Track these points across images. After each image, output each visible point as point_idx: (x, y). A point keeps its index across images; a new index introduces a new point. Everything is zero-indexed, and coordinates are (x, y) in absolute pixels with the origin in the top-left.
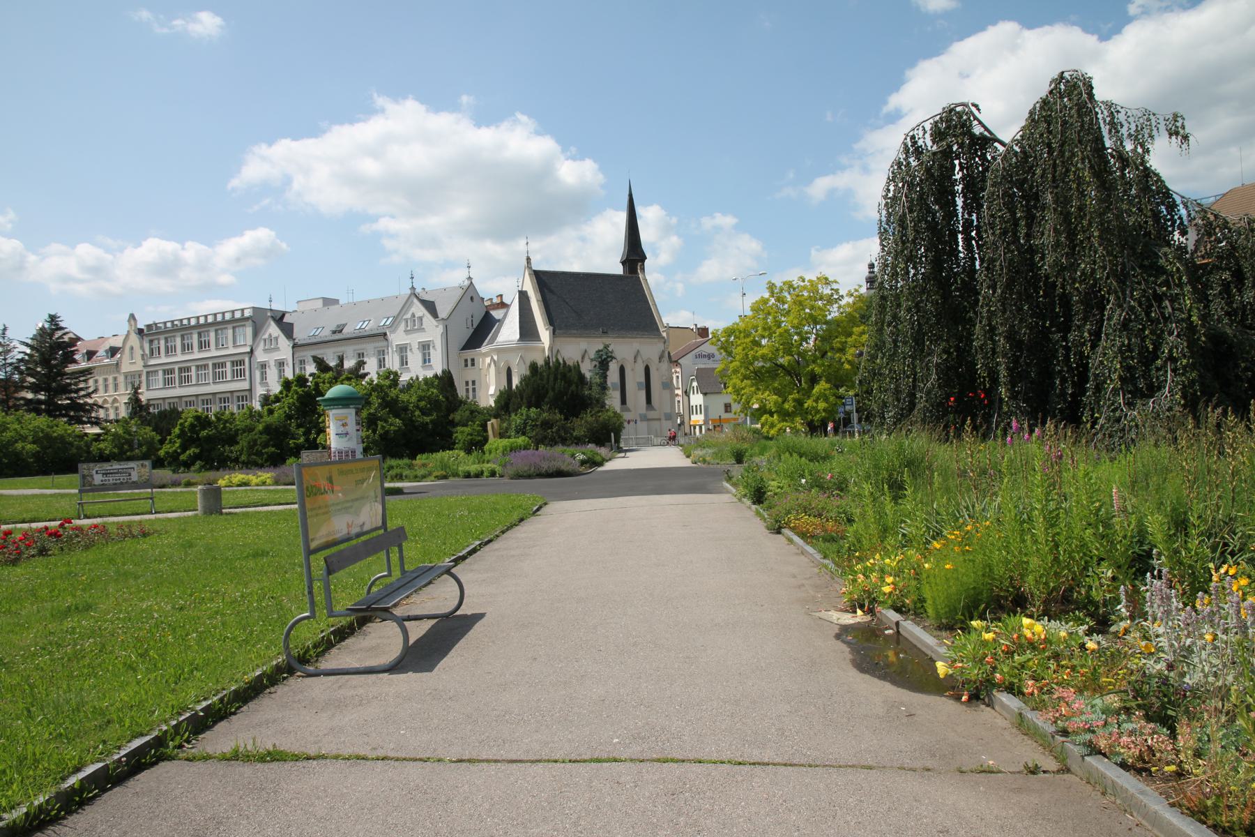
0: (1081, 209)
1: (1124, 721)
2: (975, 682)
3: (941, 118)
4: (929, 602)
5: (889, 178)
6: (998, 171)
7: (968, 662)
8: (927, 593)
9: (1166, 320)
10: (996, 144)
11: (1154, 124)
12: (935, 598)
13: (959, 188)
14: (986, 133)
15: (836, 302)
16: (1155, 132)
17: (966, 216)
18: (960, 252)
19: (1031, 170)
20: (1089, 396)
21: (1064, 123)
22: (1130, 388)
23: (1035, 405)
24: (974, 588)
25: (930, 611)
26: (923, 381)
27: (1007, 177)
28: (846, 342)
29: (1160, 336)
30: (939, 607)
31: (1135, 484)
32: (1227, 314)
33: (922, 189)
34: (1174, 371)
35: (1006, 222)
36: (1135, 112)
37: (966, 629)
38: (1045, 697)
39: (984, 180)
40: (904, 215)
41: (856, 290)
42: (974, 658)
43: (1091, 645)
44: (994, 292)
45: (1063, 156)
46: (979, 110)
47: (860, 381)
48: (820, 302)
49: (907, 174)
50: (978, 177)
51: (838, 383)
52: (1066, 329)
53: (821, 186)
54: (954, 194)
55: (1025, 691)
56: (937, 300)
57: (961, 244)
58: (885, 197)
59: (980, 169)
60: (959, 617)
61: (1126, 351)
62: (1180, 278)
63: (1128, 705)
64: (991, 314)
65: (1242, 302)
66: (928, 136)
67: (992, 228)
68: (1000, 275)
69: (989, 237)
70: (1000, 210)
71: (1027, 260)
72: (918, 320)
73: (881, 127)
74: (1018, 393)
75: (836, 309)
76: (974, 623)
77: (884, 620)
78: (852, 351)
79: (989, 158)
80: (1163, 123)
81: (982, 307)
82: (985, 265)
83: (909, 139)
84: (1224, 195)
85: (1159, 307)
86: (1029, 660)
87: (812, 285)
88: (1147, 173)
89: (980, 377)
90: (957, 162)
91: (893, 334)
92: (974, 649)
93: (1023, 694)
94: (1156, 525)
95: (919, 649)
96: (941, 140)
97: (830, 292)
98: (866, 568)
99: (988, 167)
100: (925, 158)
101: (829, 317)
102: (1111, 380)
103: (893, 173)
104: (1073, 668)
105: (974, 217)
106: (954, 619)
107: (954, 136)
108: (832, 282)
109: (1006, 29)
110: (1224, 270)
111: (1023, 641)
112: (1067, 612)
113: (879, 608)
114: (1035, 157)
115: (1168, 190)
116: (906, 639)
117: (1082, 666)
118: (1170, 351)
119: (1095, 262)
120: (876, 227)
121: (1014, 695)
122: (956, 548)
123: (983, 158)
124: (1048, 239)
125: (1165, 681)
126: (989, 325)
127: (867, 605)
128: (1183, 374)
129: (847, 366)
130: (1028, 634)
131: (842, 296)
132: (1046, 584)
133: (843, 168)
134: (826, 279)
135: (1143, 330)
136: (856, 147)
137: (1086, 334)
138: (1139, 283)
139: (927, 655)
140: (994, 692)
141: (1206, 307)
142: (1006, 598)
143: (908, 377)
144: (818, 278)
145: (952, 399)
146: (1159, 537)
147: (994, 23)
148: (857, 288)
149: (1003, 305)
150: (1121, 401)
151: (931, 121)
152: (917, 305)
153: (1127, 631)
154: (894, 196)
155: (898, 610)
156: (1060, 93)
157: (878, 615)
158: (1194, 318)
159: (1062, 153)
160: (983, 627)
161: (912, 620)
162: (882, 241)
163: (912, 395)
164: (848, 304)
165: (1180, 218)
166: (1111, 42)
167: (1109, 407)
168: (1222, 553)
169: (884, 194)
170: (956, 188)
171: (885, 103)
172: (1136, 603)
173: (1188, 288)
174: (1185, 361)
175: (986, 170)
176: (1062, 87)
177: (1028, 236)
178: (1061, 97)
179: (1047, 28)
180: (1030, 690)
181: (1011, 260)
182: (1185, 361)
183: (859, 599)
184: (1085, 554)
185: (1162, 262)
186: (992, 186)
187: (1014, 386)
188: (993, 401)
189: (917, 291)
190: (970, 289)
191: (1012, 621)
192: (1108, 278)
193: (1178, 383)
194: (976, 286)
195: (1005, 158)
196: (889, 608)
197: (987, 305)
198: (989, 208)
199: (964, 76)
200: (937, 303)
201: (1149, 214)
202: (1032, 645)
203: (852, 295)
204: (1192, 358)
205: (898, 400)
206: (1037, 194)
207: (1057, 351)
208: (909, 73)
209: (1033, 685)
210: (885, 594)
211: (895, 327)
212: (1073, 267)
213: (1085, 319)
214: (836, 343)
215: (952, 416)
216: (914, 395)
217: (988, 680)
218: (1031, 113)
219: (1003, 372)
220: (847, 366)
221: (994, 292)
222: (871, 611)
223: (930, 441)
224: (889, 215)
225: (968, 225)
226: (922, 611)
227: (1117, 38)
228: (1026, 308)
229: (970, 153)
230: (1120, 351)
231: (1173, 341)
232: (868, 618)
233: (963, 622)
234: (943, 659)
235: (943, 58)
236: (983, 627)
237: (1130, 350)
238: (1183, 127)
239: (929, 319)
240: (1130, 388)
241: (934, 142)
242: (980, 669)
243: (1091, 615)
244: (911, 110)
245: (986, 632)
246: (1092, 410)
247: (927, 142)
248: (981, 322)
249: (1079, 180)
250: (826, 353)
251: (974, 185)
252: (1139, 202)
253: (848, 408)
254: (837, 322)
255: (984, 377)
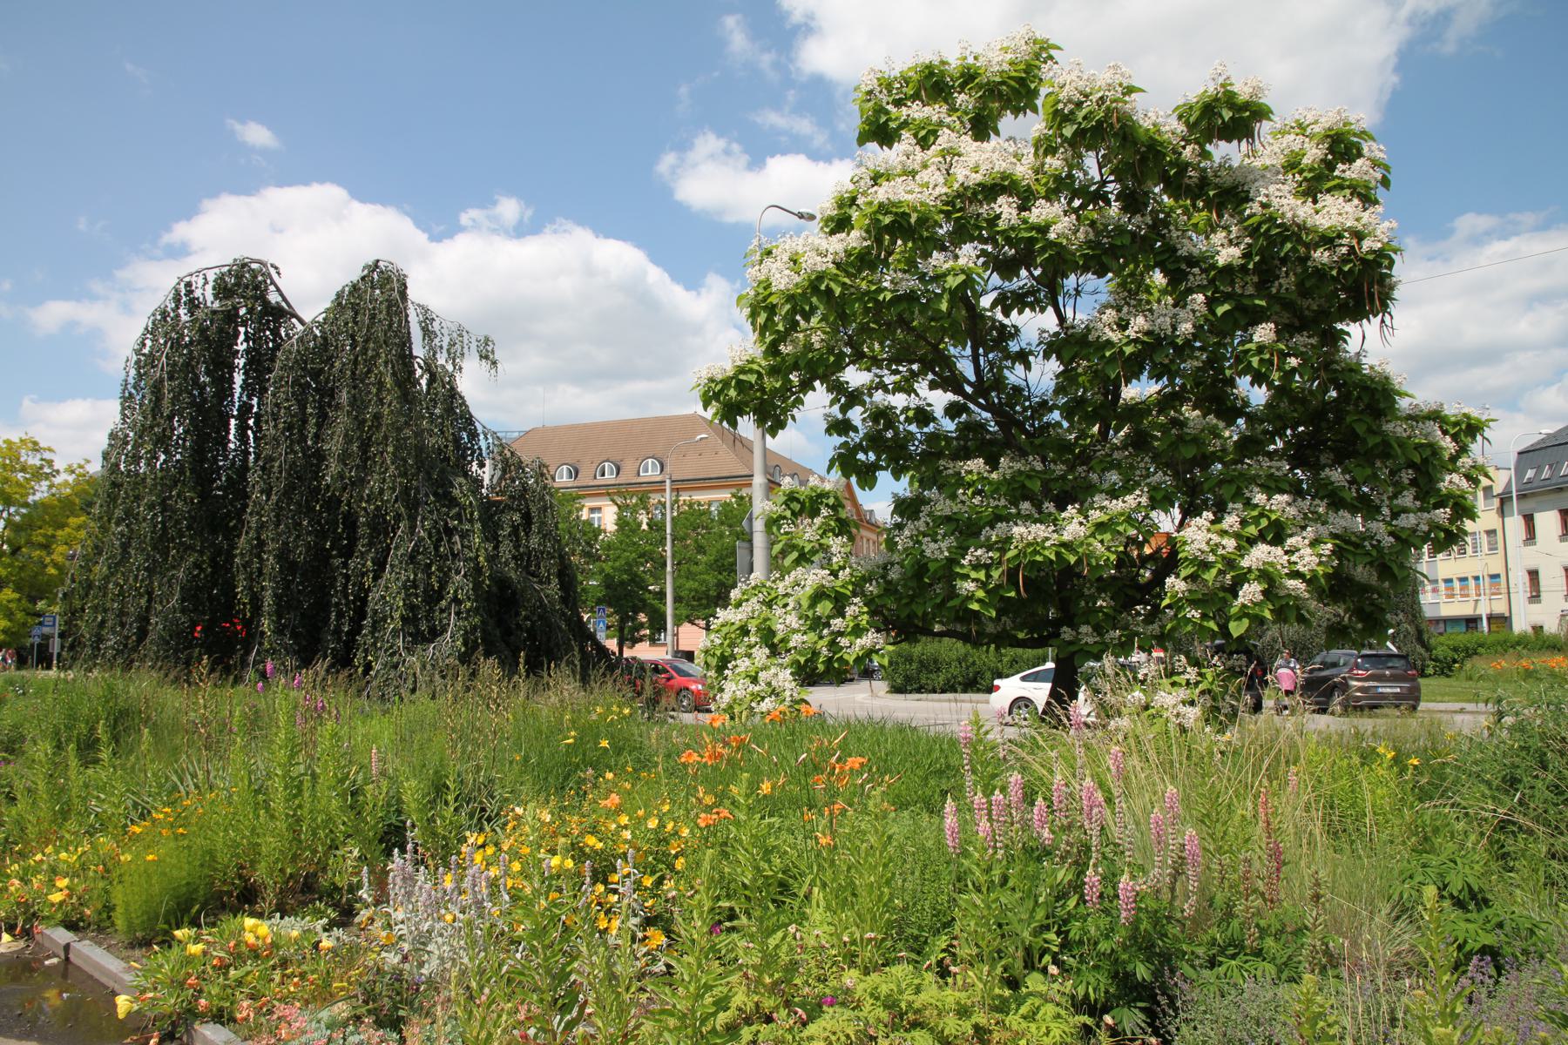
0: (377, 417)
1: (352, 1034)
2: (170, 1017)
3: (229, 271)
4: (119, 910)
5: (146, 329)
6: (291, 353)
7: (163, 989)
8: (118, 896)
9: (455, 556)
10: (294, 320)
11: (466, 341)
12: (127, 902)
13: (241, 362)
14: (284, 304)
15: (47, 479)
16: (465, 350)
17: (245, 399)
18: (229, 441)
19: (329, 360)
20: (365, 635)
21: (373, 317)
22: (412, 630)
23: (304, 643)
24: (188, 884)
25: (120, 923)
26: (161, 602)
27: (301, 361)
28: (53, 536)
29: (447, 575)
30: (133, 915)
31: (403, 741)
32: (514, 557)
33: (191, 352)
34: (458, 614)
35: (292, 416)
36: (449, 325)
37: (168, 942)
38: (263, 1020)
39: (273, 360)
40: (161, 380)
41: (81, 467)
42: (172, 982)
43: (327, 943)
44: (268, 499)
45: (366, 354)
46: (279, 273)
47: (65, 595)
48: (20, 475)
49: (173, 329)
50: (266, 354)
51: (33, 593)
52: (348, 553)
53: (54, 314)
54: (232, 368)
55: (239, 1016)
56: (192, 499)
57: (233, 431)
58: (138, 352)
59: (271, 345)
60: (161, 926)
61: (411, 587)
62: (472, 514)
63: (358, 1012)
64: (262, 526)
65: (528, 547)
66: (209, 288)
67: (275, 420)
68: (278, 479)
69: (269, 429)
70: (287, 400)
71: (312, 465)
72: (162, 522)
73: (159, 260)
74: (285, 626)
75: (45, 489)
76: (178, 933)
77: (47, 944)
78: (62, 549)
79: (283, 334)
80: (474, 344)
81: (251, 514)
82: (261, 463)
83: (182, 285)
84: (527, 433)
85: (449, 541)
86: (248, 973)
87: (10, 449)
88: (453, 394)
89: (239, 603)
90: (242, 330)
91: (123, 535)
92: (172, 970)
93: (235, 1021)
94: (412, 791)
95: (97, 981)
96: (226, 298)
97: (38, 463)
98: (26, 870)
99: (280, 345)
100: (199, 314)
101: (31, 499)
102: (392, 618)
103: (154, 323)
104: (302, 976)
105: (255, 401)
106: (152, 929)
107: (243, 297)
108: (45, 449)
109: (331, 193)
110: (516, 510)
111: (243, 948)
112: (305, 904)
113: (40, 927)
114: (336, 347)
115: (471, 416)
116: (79, 968)
117: (313, 972)
118: (456, 591)
119: (384, 480)
120: (120, 389)
121: (223, 1024)
122: (164, 832)
123: (276, 333)
124: (334, 446)
125: (398, 976)
126: (258, 538)
127: (20, 925)
128: (466, 619)
129: (52, 571)
130: (250, 938)
131: (58, 472)
132: (282, 871)
133: (94, 298)
134: (35, 443)
135: (429, 566)
136: (120, 274)
137: (369, 563)
138: (431, 512)
139: (107, 988)
140: (197, 1026)
141: (496, 548)
142: (230, 894)
143: (141, 596)
144: (21, 440)
145: (199, 629)
146: (413, 805)
147: (322, 181)
148: (83, 463)
149: (277, 516)
150: (401, 644)
151: (217, 271)
152: (163, 503)
153: (372, 920)
154: (151, 352)
155: (71, 926)
156: (372, 282)
157: (38, 937)
158: (481, 559)
159: (365, 350)
160: (190, 937)
161: (92, 939)
162: (123, 409)
163: (144, 620)
164: (66, 483)
165: (480, 449)
166: (440, 245)
167: (386, 651)
168: (480, 819)
169: (136, 347)
170: (236, 361)
171: (168, 229)
172: (381, 882)
173: (478, 526)
174: (469, 604)
175: (277, 347)
176: (376, 276)
177: (317, 437)
178: (373, 288)
179: (379, 208)
180: (244, 1014)
181: (294, 463)
182: (469, 604)
183: (8, 917)
184: (331, 831)
185: (456, 492)
186: (281, 369)
187: (280, 617)
188: (252, 635)
189: (170, 480)
190: (238, 486)
191: (229, 923)
192: (396, 501)
193: (460, 629)
194: (245, 487)
195: (301, 340)
196: (57, 925)
197: (258, 513)
198: (274, 395)
199: (277, 229)
200: (193, 503)
201: (451, 438)
202: (255, 953)
203: (73, 472)
204: (476, 601)
205: (123, 625)
206: (332, 389)
207: (335, 579)
208: (207, 204)
209: (249, 1006)
210: (53, 905)
211: (127, 526)
212: (362, 482)
213: (370, 545)
214: (38, 537)
215: (197, 650)
216: (148, 621)
217: (189, 1010)
218: (339, 295)
219: (268, 600)
220: (52, 571)
221: (268, 499)
222: (27, 933)
223: (160, 684)
224: (140, 376)
225: (245, 409)
226: (107, 924)
227: (447, 242)
228: (305, 523)
229: (260, 323)
230: (405, 587)
231: (459, 582)
232: (21, 944)
233: (166, 933)
234: (128, 990)
235: (252, 200)
236: (190, 937)
237: (416, 587)
238: (493, 352)
239: (178, 522)
240: (412, 630)
241: (216, 296)
242: (178, 996)
243: (336, 906)
244: (203, 249)
245: (195, 943)
246: (366, 651)
247: (206, 294)
248: (247, 533)
249: (380, 385)
250: (19, 548)
251: (259, 362)
252: (442, 424)
253: (46, 630)
254: (42, 506)
255: (244, 604)
